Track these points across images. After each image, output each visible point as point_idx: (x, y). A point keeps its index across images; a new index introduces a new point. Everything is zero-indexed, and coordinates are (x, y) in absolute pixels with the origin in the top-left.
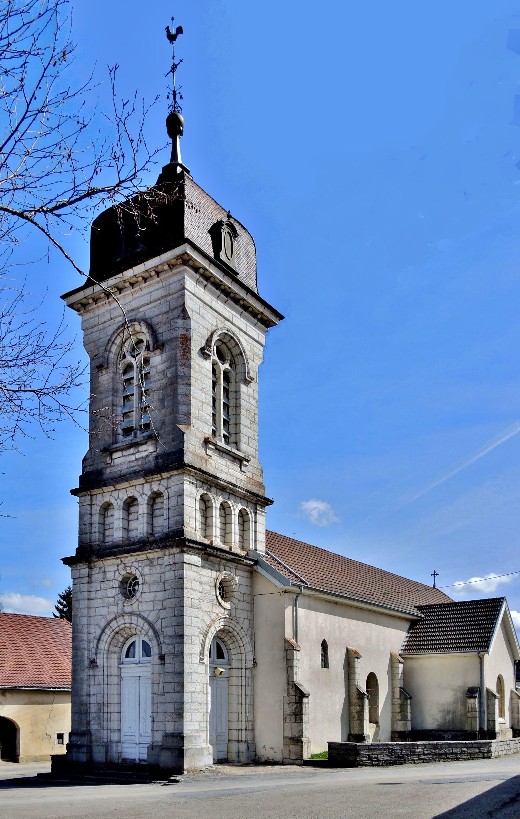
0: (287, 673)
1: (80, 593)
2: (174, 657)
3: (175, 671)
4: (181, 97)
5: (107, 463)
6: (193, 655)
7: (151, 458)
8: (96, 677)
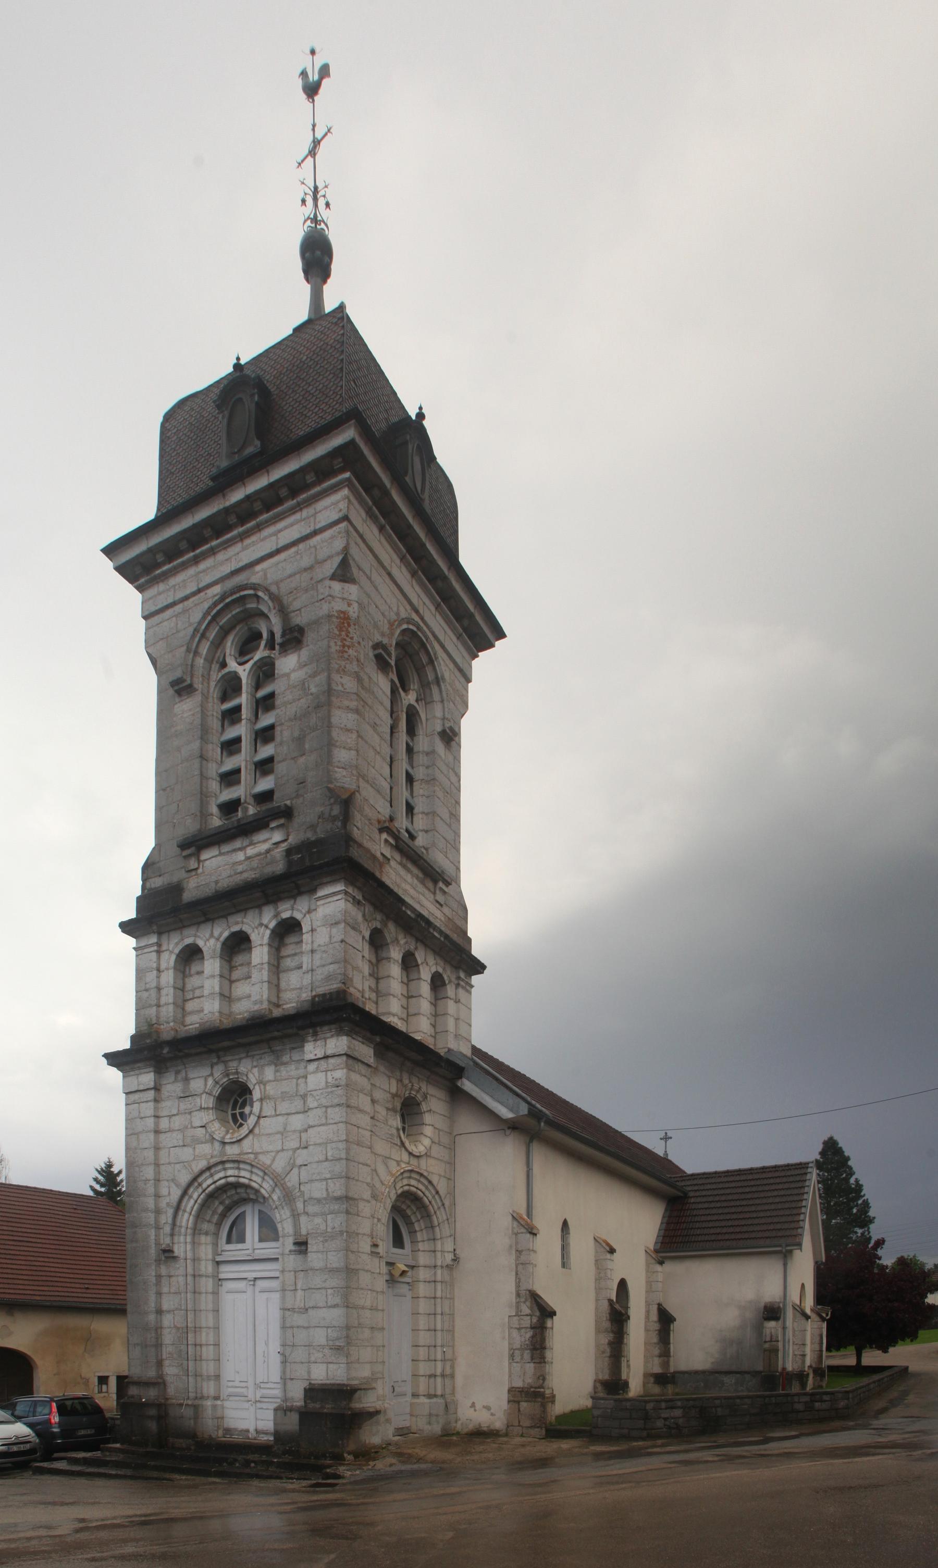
0: (517, 1274)
1: (139, 1120)
2: (326, 1241)
3: (329, 1266)
4: (328, 205)
6: (360, 1236)
7: (279, 852)
8: (173, 1279)
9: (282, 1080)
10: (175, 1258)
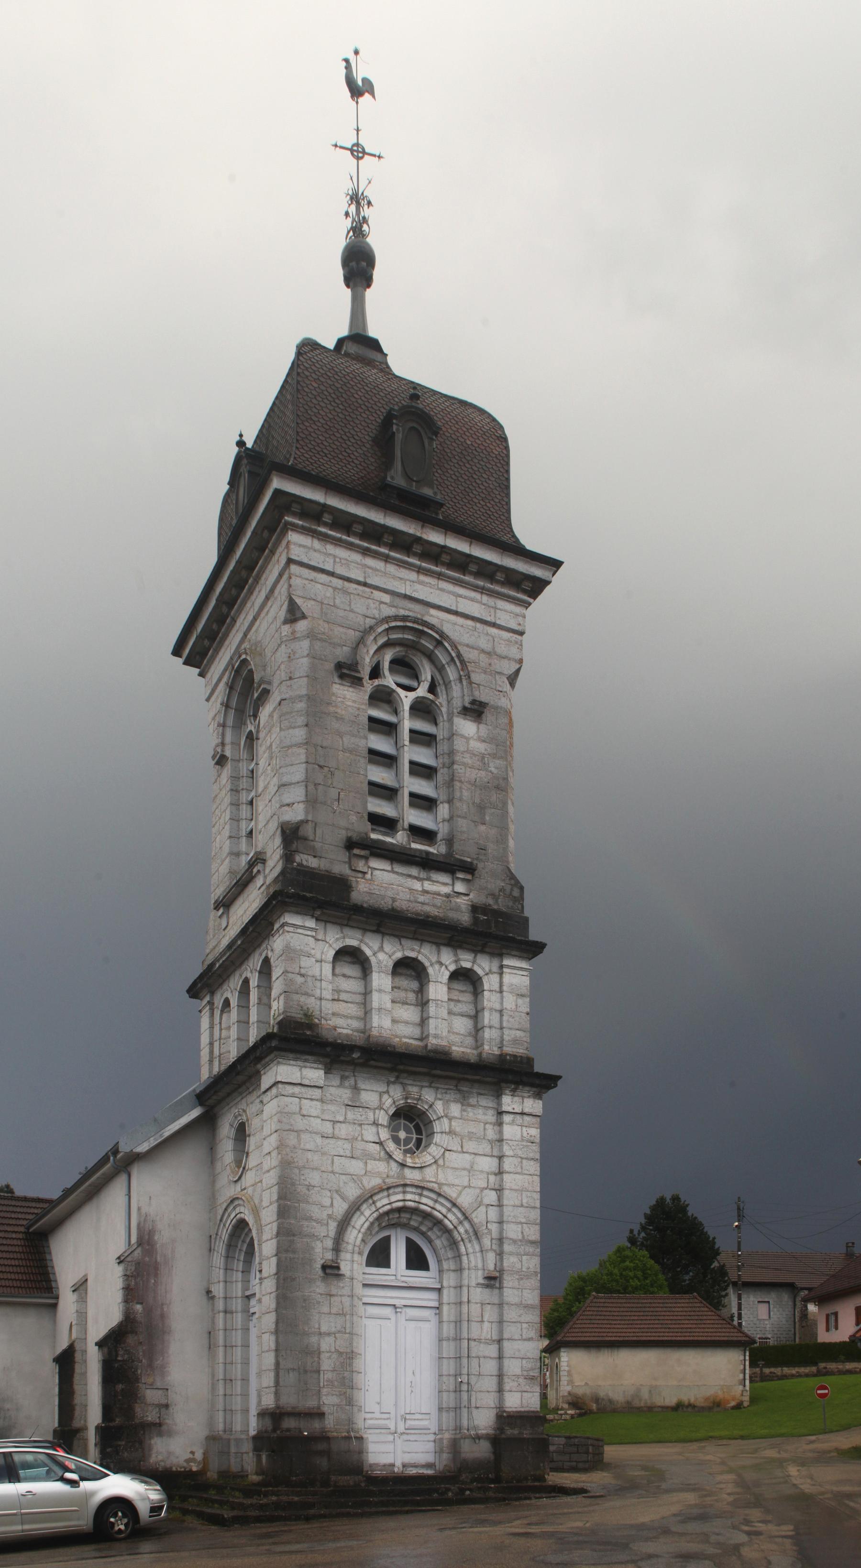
2: (522, 1279)
5: (358, 869)
9: (468, 1120)
10: (339, 1276)
